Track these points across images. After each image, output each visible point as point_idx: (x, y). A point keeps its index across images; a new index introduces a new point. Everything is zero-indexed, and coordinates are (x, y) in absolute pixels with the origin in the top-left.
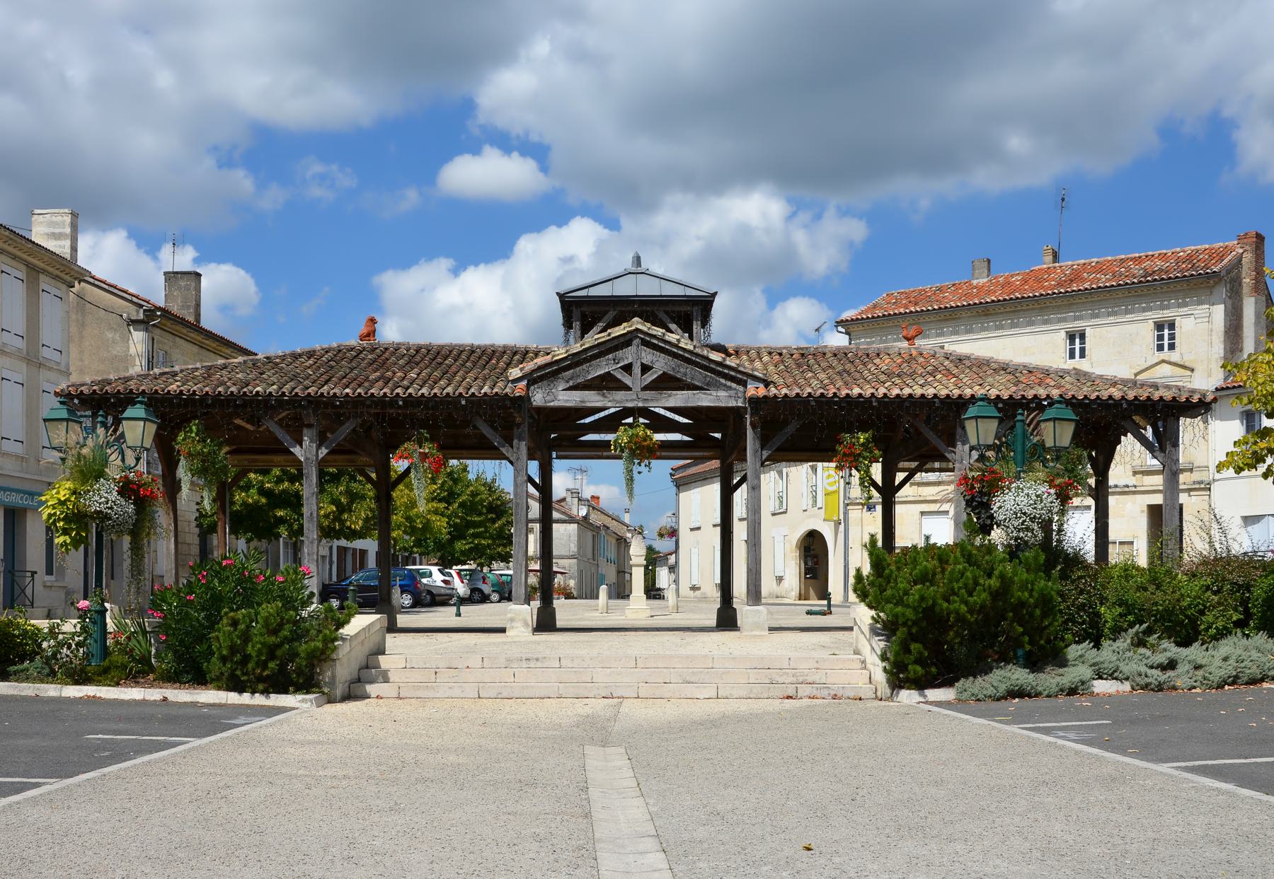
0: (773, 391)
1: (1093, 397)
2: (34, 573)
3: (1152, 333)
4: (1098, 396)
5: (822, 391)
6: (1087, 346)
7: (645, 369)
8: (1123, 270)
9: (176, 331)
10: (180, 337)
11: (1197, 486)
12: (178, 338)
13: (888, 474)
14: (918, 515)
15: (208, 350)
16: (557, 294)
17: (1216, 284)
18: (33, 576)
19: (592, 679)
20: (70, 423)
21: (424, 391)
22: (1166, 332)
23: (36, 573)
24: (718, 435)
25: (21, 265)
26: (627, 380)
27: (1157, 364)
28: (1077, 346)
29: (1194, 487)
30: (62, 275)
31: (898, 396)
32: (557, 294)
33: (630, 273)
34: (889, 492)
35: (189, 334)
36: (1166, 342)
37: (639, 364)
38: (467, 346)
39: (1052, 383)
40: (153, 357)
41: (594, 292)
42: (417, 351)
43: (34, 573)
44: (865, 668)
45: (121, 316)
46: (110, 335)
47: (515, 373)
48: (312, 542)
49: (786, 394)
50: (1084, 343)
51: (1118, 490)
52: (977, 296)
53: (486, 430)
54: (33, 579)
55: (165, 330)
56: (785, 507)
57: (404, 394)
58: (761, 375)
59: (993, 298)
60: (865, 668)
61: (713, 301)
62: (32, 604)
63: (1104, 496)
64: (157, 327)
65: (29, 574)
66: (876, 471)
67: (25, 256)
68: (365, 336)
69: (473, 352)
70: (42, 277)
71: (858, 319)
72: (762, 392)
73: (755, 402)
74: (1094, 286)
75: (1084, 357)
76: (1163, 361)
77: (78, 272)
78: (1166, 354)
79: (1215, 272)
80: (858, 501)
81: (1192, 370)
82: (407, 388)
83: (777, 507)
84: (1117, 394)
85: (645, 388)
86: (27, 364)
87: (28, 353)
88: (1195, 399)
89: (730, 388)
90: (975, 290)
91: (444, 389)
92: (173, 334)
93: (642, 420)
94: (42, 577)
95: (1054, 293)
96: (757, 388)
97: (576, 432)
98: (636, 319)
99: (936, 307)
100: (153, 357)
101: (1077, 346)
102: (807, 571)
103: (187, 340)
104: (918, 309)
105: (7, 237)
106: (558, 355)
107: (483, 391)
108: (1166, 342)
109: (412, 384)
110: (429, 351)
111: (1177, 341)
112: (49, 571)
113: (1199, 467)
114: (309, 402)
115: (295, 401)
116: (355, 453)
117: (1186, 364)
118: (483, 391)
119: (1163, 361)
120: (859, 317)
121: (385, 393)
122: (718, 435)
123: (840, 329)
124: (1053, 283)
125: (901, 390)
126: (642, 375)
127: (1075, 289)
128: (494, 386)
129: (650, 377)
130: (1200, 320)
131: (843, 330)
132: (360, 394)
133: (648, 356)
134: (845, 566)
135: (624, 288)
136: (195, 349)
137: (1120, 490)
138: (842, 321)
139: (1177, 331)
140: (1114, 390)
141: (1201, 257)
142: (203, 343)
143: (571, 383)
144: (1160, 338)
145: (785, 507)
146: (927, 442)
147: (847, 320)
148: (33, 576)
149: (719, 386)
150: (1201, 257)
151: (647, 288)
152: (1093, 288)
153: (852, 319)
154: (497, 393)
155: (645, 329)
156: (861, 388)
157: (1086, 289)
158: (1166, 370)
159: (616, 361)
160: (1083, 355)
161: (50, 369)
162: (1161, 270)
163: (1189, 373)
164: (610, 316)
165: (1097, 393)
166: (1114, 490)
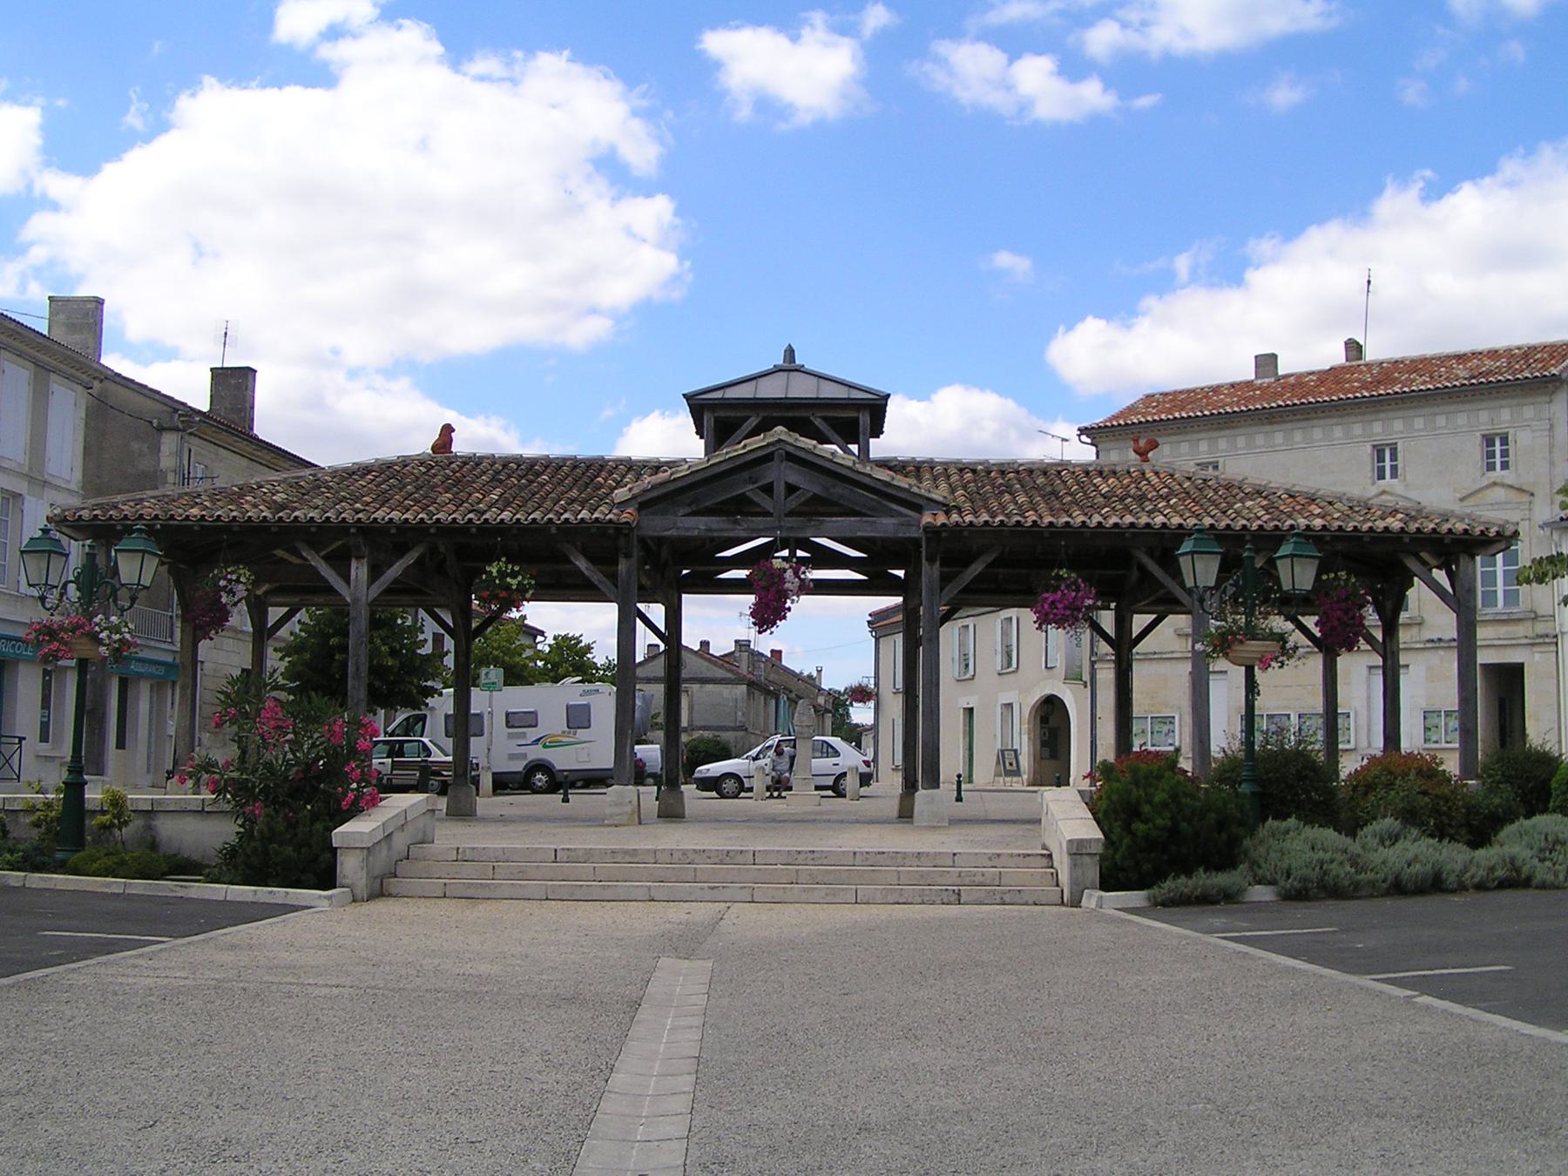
0: (955, 517)
1: (1365, 527)
2: (21, 739)
3: (1479, 449)
4: (1371, 528)
5: (1019, 518)
6: (1400, 463)
7: (791, 489)
8: (1443, 369)
9: (219, 440)
10: (224, 448)
11: (1541, 640)
12: (221, 449)
13: (1122, 622)
14: (1365, 671)
15: (261, 464)
16: (684, 395)
17: (1557, 388)
18: (20, 742)
19: (899, 879)
20: (52, 555)
21: (506, 515)
22: (1498, 447)
23: (24, 739)
24: (901, 573)
25: (28, 363)
26: (765, 502)
27: (1487, 487)
28: (1388, 463)
29: (1537, 641)
30: (78, 374)
31: (1116, 525)
32: (684, 395)
33: (780, 370)
34: (1124, 646)
35: (237, 444)
36: (1498, 459)
37: (783, 483)
38: (569, 459)
39: (1318, 511)
40: (189, 473)
41: (731, 393)
42: (575, 467)
43: (21, 739)
44: (1058, 885)
45: (151, 422)
46: (135, 446)
47: (621, 494)
48: (357, 704)
49: (971, 522)
50: (1396, 460)
51: (1442, 644)
52: (1261, 398)
53: (582, 564)
54: (20, 747)
55: (206, 440)
56: (1014, 665)
57: (479, 520)
58: (941, 499)
59: (1281, 403)
60: (1058, 885)
61: (886, 405)
62: (19, 777)
63: (1393, 652)
64: (196, 436)
65: (17, 740)
66: (1107, 620)
67: (32, 352)
68: (440, 448)
69: (575, 467)
70: (53, 377)
71: (1106, 426)
72: (941, 519)
73: (933, 532)
74: (1406, 389)
75: (1396, 477)
76: (1495, 484)
77: (96, 370)
78: (1498, 474)
79: (1554, 375)
80: (1108, 658)
81: (1532, 495)
82: (484, 512)
83: (1005, 665)
84: (1395, 524)
85: (791, 514)
86: (29, 482)
87: (31, 469)
88: (1493, 532)
89: (900, 514)
90: (1258, 392)
91: (530, 514)
92: (215, 444)
93: (800, 553)
94: (33, 744)
95: (1356, 397)
96: (935, 514)
97: (713, 568)
98: (779, 428)
99: (1206, 413)
100: (189, 473)
101: (1388, 463)
102: (1044, 744)
103: (234, 452)
104: (1184, 415)
105: (13, 330)
106: (681, 471)
107: (579, 517)
108: (1498, 459)
109: (490, 507)
110: (519, 466)
111: (1511, 459)
112: (44, 737)
113: (1543, 616)
114: (359, 529)
115: (342, 528)
116: (425, 594)
117: (1524, 487)
118: (579, 517)
119: (1495, 484)
120: (1108, 424)
121: (454, 519)
122: (901, 573)
123: (1084, 438)
124: (1356, 384)
125: (1121, 518)
126: (786, 498)
127: (1382, 392)
128: (596, 510)
129: (794, 502)
130: (1538, 434)
131: (1089, 441)
132: (422, 519)
133: (794, 476)
134: (1092, 742)
135: (771, 390)
136: (245, 462)
137: (1446, 645)
138: (1086, 428)
139: (1511, 447)
140: (1393, 519)
141: (1539, 356)
142: (253, 455)
143: (694, 508)
144: (1491, 455)
145: (1014, 665)
146: (1162, 586)
147: (1093, 428)
148: (20, 742)
149: (891, 513)
150: (1539, 356)
151: (801, 389)
152: (1404, 392)
153: (1100, 427)
154: (597, 518)
155: (790, 440)
156: (1070, 516)
157: (1396, 393)
158: (1499, 494)
159: (752, 480)
160: (1394, 475)
161: (57, 488)
162: (1489, 373)
163: (1526, 498)
164: (753, 422)
165: (1370, 524)
166: (1138, 657)
